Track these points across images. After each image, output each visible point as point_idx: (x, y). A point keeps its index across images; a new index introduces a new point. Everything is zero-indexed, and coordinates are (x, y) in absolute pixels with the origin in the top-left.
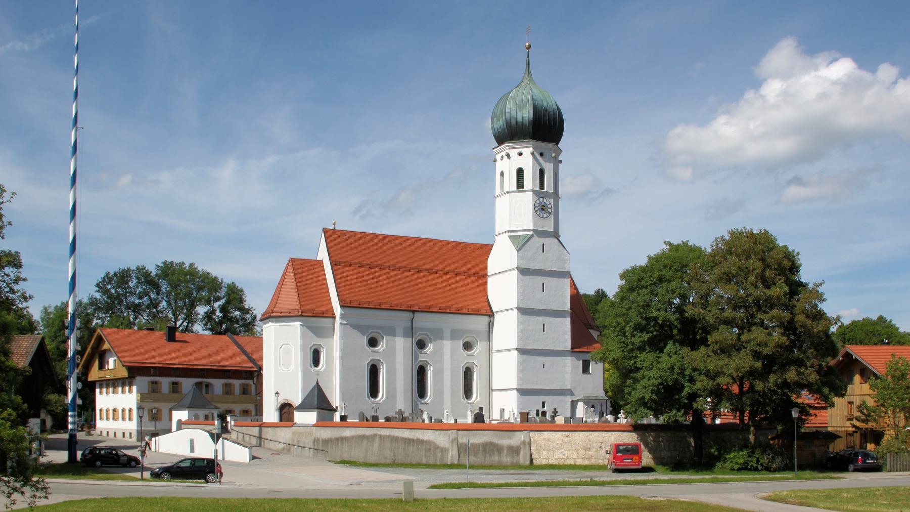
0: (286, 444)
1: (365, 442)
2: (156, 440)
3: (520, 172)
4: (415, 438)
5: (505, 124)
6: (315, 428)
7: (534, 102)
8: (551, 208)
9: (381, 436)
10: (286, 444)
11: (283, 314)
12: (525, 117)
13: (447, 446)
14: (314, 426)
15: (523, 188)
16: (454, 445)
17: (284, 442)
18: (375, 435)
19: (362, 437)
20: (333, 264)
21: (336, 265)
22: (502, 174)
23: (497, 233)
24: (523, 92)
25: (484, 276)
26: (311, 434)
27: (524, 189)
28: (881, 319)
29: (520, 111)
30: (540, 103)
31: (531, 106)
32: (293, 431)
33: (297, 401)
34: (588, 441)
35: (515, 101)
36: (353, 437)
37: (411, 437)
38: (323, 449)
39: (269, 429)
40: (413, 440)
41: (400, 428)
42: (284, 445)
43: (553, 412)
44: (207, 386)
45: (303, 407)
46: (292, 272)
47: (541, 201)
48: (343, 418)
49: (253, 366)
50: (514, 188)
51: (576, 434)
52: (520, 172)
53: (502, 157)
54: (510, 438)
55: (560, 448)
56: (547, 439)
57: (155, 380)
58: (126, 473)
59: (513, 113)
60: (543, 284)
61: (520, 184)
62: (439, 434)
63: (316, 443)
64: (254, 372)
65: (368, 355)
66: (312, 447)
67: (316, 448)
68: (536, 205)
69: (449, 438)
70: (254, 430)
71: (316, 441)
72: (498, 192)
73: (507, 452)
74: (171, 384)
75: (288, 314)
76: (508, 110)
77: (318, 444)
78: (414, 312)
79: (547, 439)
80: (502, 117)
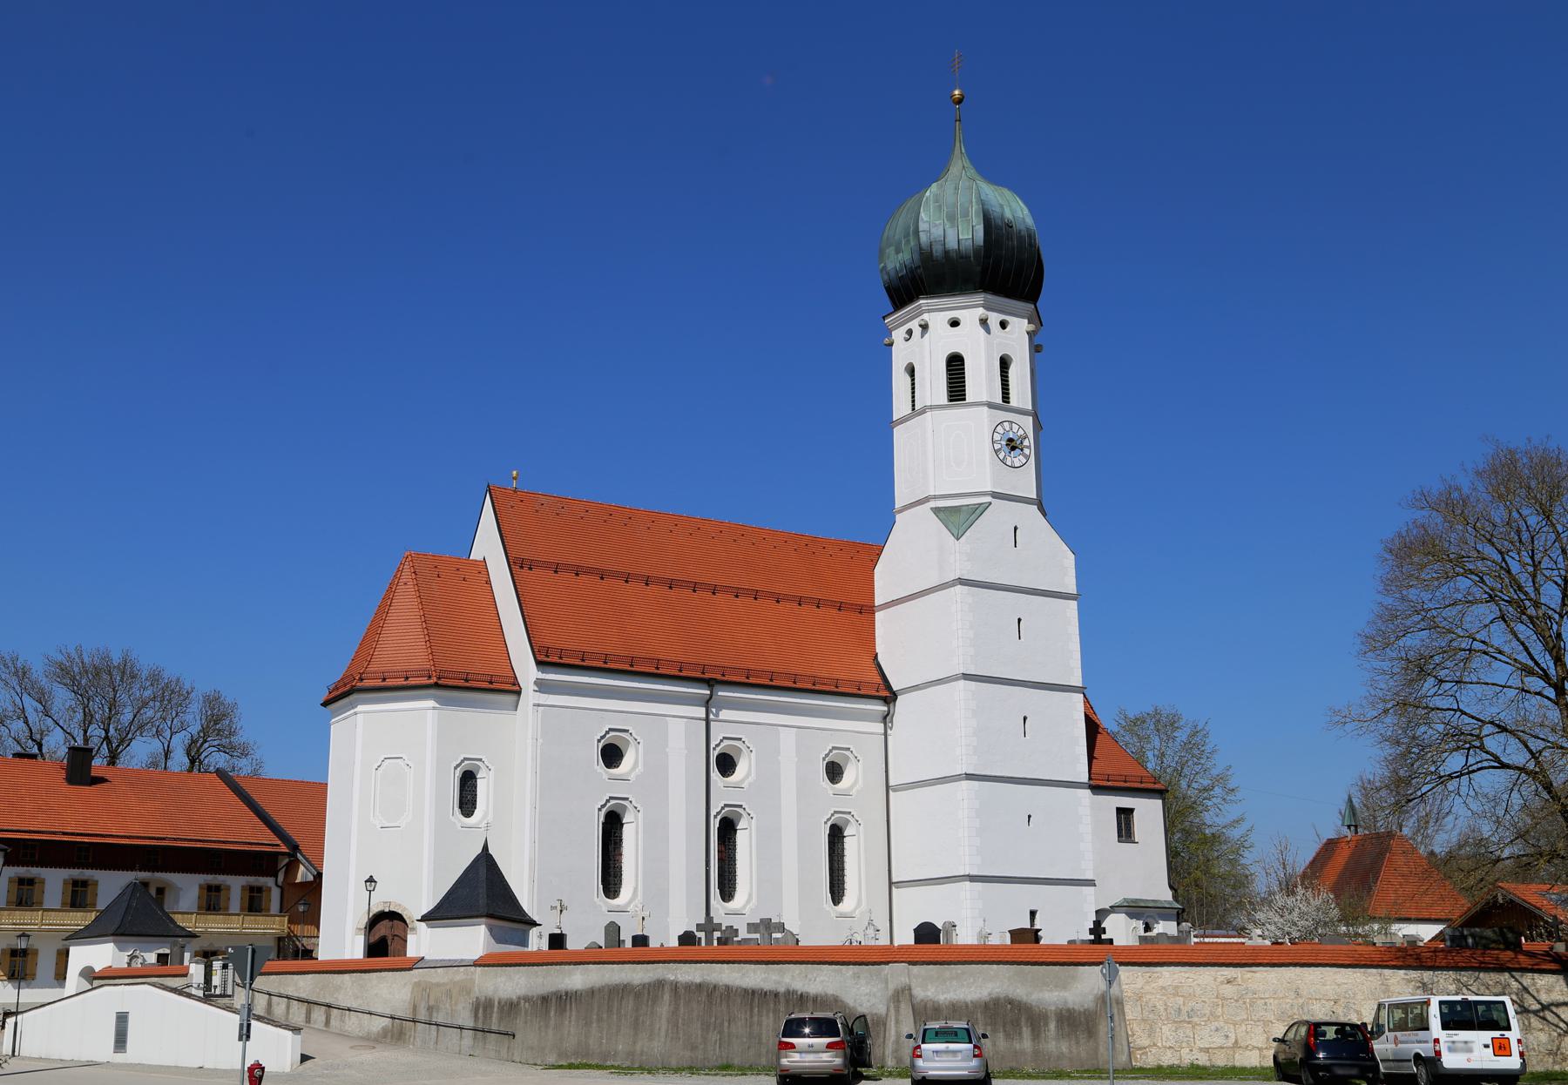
0: (392, 1018)
1: (629, 1004)
2: (16, 1024)
3: (955, 364)
4: (782, 989)
5: (916, 257)
6: (479, 969)
7: (986, 207)
8: (1029, 447)
9: (675, 987)
10: (392, 1018)
11: (389, 683)
13: (881, 1009)
14: (476, 964)
15: (964, 399)
16: (903, 1006)
17: (388, 1012)
18: (659, 984)
19: (619, 992)
20: (516, 564)
21: (522, 567)
22: (911, 371)
23: (898, 505)
24: (956, 188)
25: (867, 610)
26: (465, 989)
27: (967, 401)
29: (952, 226)
30: (998, 210)
31: (977, 215)
33: (417, 899)
34: (1293, 995)
36: (592, 992)
37: (767, 986)
38: (502, 1029)
39: (347, 977)
40: (776, 995)
41: (734, 962)
42: (387, 1021)
43: (1091, 931)
44: (161, 891)
45: (446, 912)
46: (411, 588)
47: (1008, 429)
48: (557, 941)
49: (279, 842)
50: (942, 397)
51: (1258, 975)
52: (955, 364)
53: (910, 332)
54: (1064, 986)
55: (1213, 1016)
56: (1170, 990)
57: (29, 876)
58: (1020, 198)
59: (937, 233)
61: (956, 390)
62: (857, 976)
63: (481, 1011)
64: (280, 857)
65: (602, 785)
66: (471, 1024)
67: (480, 1026)
68: (997, 437)
69: (887, 988)
70: (301, 984)
71: (483, 1007)
72: (900, 407)
73: (1057, 1027)
74: (8, 956)
75: (401, 682)
76: (922, 226)
77: (487, 1016)
78: (710, 683)
79: (1170, 990)
80: (908, 241)
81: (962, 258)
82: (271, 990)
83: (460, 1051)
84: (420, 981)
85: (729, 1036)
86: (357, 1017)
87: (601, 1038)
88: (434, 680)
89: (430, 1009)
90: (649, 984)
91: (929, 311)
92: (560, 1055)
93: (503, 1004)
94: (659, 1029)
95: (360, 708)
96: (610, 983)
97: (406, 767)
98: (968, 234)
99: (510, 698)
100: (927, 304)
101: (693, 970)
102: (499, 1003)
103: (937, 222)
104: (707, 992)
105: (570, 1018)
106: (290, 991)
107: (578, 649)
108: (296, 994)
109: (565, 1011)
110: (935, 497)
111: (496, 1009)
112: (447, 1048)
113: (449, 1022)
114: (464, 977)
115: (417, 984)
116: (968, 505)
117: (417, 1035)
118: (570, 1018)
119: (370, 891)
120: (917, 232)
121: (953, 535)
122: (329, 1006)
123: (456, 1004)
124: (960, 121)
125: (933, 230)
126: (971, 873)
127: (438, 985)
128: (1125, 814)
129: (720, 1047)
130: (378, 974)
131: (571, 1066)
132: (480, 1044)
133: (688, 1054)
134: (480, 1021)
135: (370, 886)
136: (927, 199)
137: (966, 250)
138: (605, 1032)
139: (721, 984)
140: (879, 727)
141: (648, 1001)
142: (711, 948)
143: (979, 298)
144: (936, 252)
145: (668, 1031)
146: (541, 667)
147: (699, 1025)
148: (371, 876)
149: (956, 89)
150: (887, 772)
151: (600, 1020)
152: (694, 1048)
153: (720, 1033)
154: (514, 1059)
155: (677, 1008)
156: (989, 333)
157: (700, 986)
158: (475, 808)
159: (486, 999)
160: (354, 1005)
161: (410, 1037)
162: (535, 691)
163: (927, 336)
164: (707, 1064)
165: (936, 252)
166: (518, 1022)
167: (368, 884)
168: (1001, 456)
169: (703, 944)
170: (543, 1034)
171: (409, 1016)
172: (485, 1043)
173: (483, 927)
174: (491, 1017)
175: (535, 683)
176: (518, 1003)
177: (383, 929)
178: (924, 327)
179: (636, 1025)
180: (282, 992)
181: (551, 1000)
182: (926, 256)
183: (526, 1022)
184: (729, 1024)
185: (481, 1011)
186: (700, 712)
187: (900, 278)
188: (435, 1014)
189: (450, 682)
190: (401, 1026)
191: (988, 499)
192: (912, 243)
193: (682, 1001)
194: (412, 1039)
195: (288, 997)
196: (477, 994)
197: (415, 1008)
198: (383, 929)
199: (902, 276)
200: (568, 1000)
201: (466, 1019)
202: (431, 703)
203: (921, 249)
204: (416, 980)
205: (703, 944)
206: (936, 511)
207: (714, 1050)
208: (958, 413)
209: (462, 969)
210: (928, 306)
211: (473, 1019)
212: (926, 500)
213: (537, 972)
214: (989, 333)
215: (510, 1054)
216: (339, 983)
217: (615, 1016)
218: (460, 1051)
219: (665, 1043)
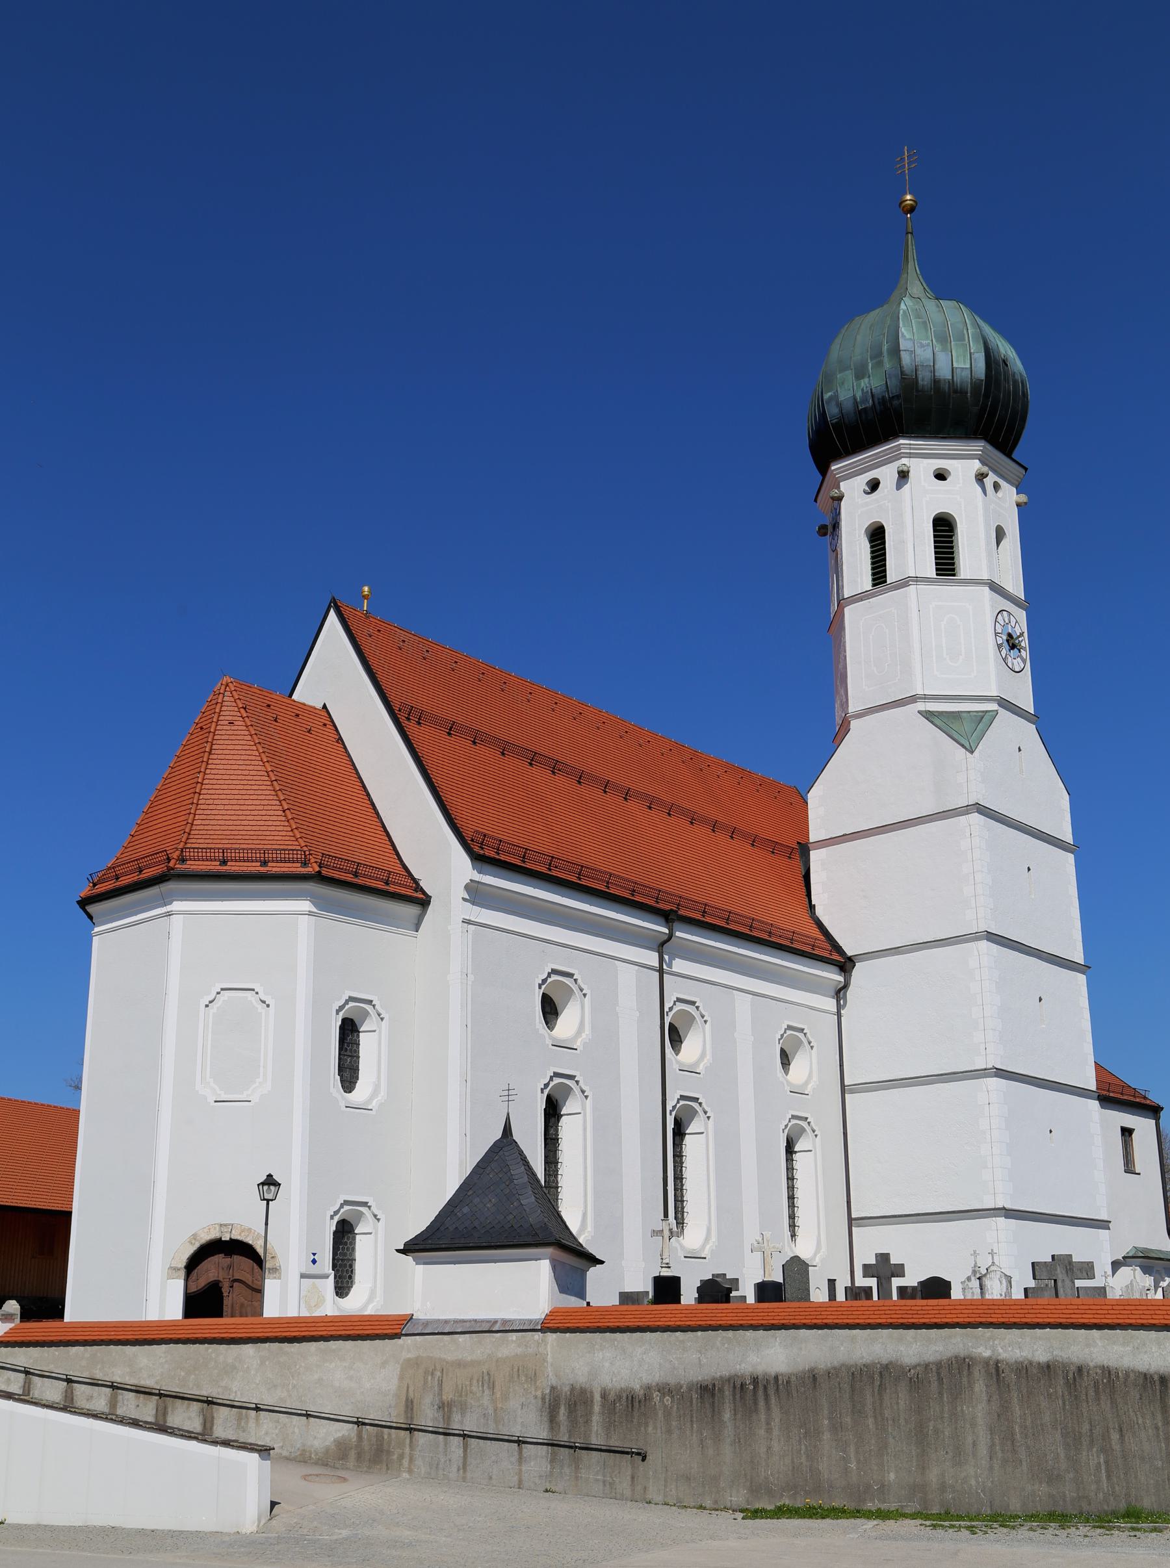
0: (359, 1423)
1: (900, 1400)
3: (944, 527)
6: (551, 1337)
9: (995, 1370)
12: (962, 369)
17: (347, 1411)
18: (962, 1365)
23: (852, 708)
26: (523, 1371)
28: (1102, 1108)
29: (944, 350)
32: (406, 1355)
35: (925, 323)
36: (812, 1378)
38: (615, 1442)
39: (249, 1349)
50: (929, 567)
52: (944, 527)
60: (250, 1101)
61: (946, 563)
63: (563, 1412)
66: (543, 1434)
67: (564, 1437)
78: (668, 917)
80: (880, 364)
81: (956, 391)
82: (73, 1373)
83: (520, 1482)
84: (417, 1358)
85: (1124, 1457)
86: (500, 1431)
87: (846, 1460)
88: (313, 868)
89: (445, 1407)
90: (939, 1365)
91: (910, 455)
92: (755, 1490)
93: (612, 1397)
94: (974, 1444)
95: (177, 906)
96: (852, 1362)
97: (261, 1008)
98: (965, 362)
99: (412, 910)
100: (910, 446)
101: (1028, 1339)
102: (604, 1396)
103: (924, 342)
104: (1066, 1377)
105: (768, 1423)
106: (118, 1375)
107: (521, 843)
108: (130, 1380)
109: (756, 1410)
110: (926, 698)
111: (597, 1408)
112: (491, 1478)
113: (491, 1429)
114: (519, 1351)
115: (413, 1364)
116: (969, 712)
117: (417, 1453)
118: (768, 1423)
119: (268, 1201)
120: (896, 351)
121: (963, 746)
122: (210, 1402)
123: (505, 1397)
124: (911, 233)
125: (919, 351)
126: (1008, 1206)
127: (460, 1364)
128: (1127, 1132)
129: (1109, 1477)
130: (322, 1344)
131: (781, 1512)
132: (567, 1470)
133: (1043, 1489)
134: (563, 1429)
135: (269, 1191)
136: (904, 311)
137: (961, 385)
138: (852, 1449)
139: (1092, 1364)
140: (830, 1004)
141: (941, 1393)
142: (887, 1302)
143: (977, 447)
144: (923, 380)
145: (993, 1445)
146: (479, 864)
147: (1058, 1436)
148: (270, 1176)
149: (906, 194)
150: (841, 1065)
151: (836, 1428)
152: (1053, 1478)
153: (1106, 1450)
154: (649, 1497)
155: (1005, 1407)
156: (986, 496)
157: (1048, 1369)
158: (358, 1079)
159: (573, 1389)
160: (268, 1400)
161: (401, 1457)
162: (464, 899)
163: (906, 488)
164: (1085, 1507)
165: (923, 380)
166: (650, 1429)
167: (266, 1188)
168: (1004, 652)
169: (875, 1297)
170: (711, 1452)
171: (397, 1417)
172: (577, 1468)
173: (545, 1266)
174: (588, 1422)
175: (467, 888)
176: (647, 1397)
177: (212, 1270)
178: (903, 475)
179: (921, 1437)
180: (99, 1375)
181: (721, 1390)
182: (909, 384)
183: (669, 1432)
184: (1122, 1435)
185: (563, 1412)
186: (652, 958)
187: (860, 412)
188: (456, 1417)
189: (336, 875)
190: (380, 1438)
191: (993, 706)
192: (887, 365)
193: (1015, 1394)
194: (406, 1462)
195: (113, 1386)
196: (553, 1381)
197: (410, 1405)
198: (212, 1270)
199: (865, 409)
200: (761, 1392)
201: (532, 1425)
202: (305, 905)
203: (902, 373)
204: (410, 1356)
205: (875, 1297)
206: (929, 715)
207: (1098, 1482)
208: (946, 591)
209: (514, 1336)
210: (910, 449)
211: (546, 1425)
212: (913, 699)
213: (683, 1342)
214: (986, 496)
215: (639, 1488)
216: (230, 1361)
217: (871, 1421)
218: (520, 1482)
219: (991, 1468)
